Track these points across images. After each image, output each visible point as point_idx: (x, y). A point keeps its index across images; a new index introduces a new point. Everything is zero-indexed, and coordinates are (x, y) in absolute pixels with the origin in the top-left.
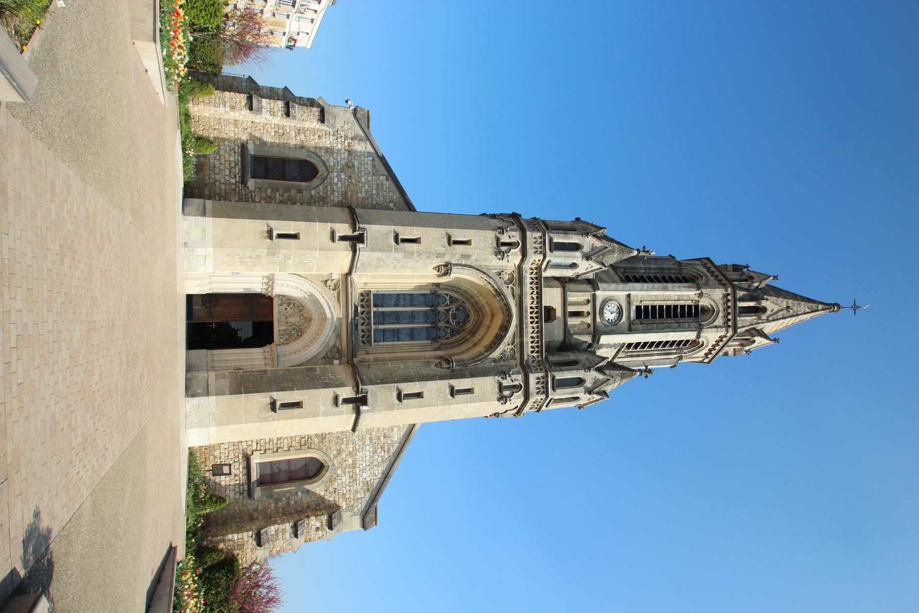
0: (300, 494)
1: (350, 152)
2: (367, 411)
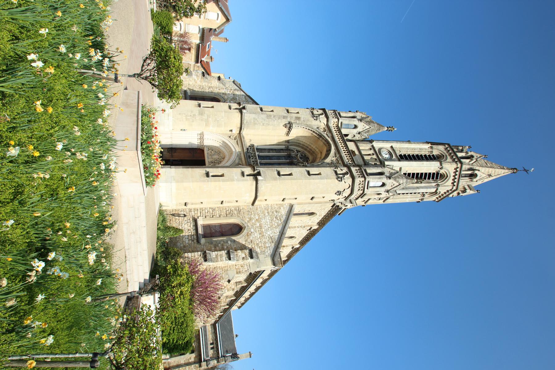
0: (229, 242)
1: (234, 94)
2: (262, 180)
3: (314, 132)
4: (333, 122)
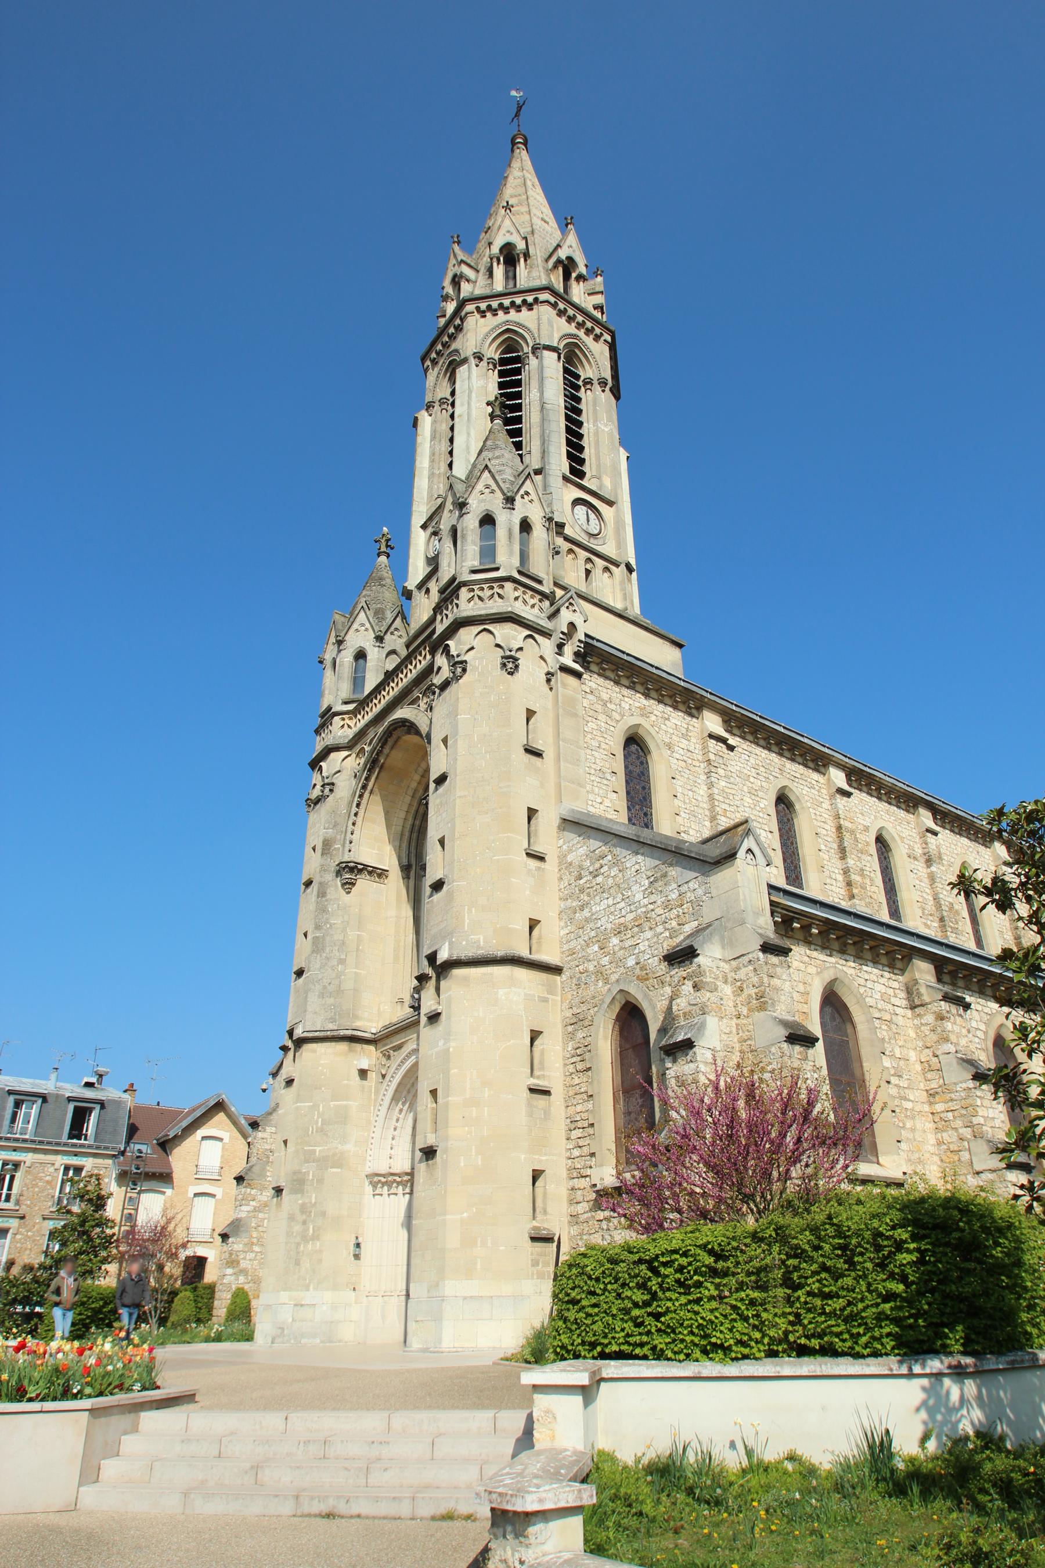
3: (364, 787)
4: (341, 731)
